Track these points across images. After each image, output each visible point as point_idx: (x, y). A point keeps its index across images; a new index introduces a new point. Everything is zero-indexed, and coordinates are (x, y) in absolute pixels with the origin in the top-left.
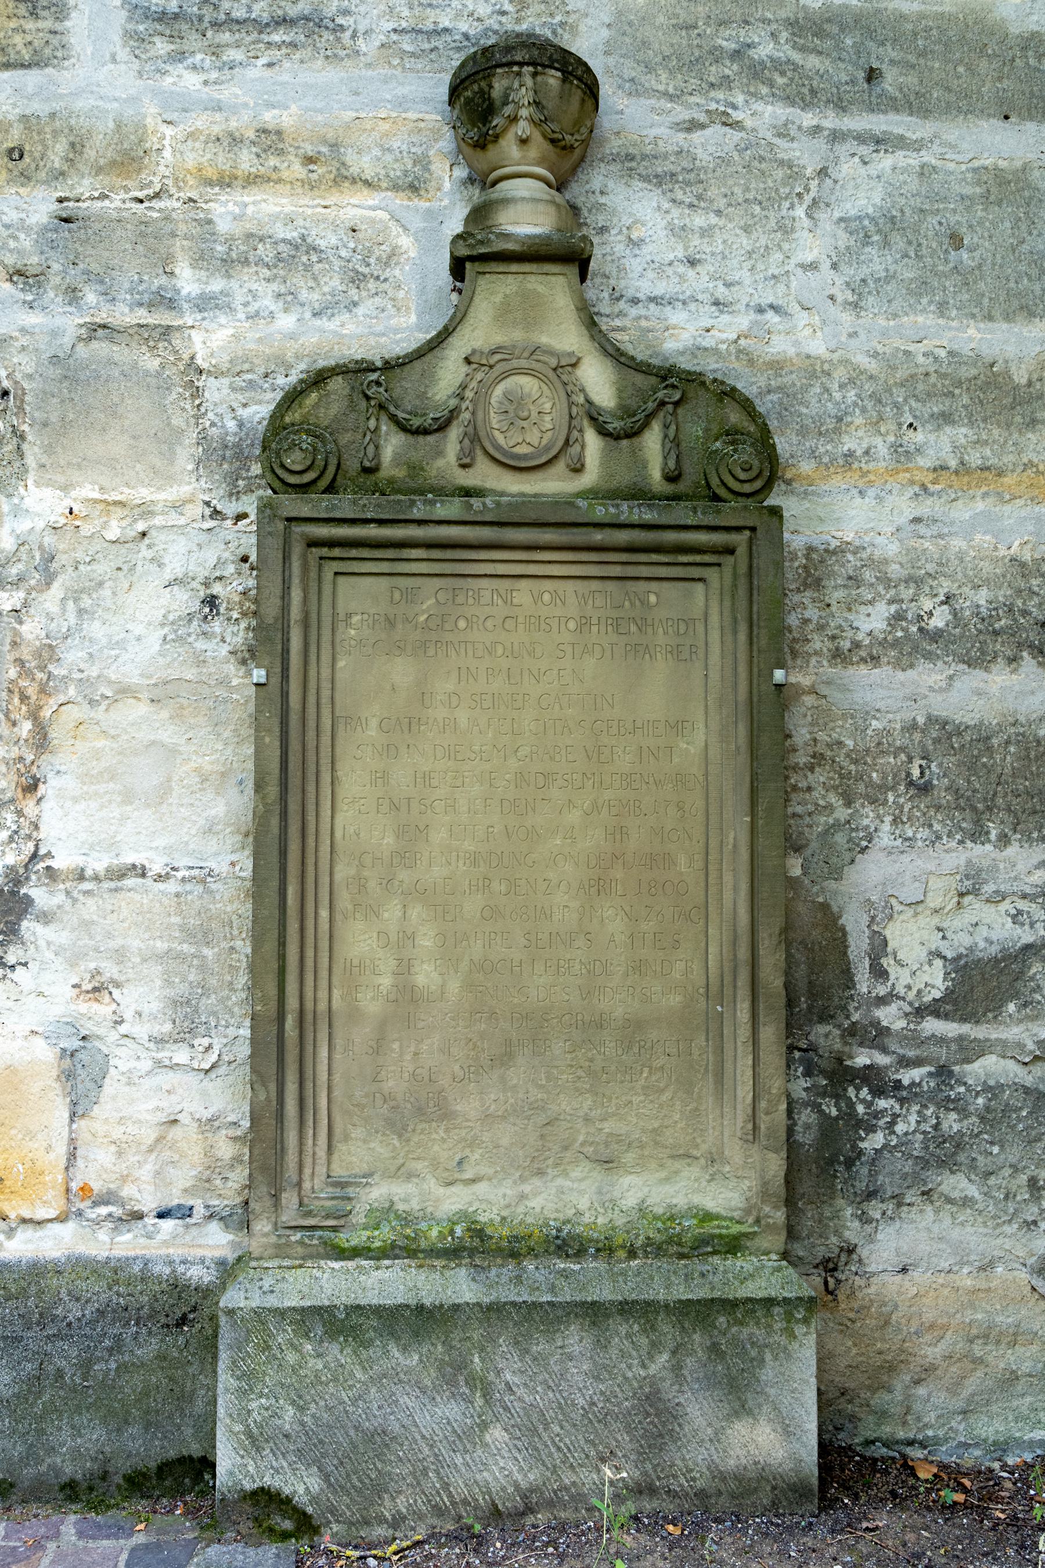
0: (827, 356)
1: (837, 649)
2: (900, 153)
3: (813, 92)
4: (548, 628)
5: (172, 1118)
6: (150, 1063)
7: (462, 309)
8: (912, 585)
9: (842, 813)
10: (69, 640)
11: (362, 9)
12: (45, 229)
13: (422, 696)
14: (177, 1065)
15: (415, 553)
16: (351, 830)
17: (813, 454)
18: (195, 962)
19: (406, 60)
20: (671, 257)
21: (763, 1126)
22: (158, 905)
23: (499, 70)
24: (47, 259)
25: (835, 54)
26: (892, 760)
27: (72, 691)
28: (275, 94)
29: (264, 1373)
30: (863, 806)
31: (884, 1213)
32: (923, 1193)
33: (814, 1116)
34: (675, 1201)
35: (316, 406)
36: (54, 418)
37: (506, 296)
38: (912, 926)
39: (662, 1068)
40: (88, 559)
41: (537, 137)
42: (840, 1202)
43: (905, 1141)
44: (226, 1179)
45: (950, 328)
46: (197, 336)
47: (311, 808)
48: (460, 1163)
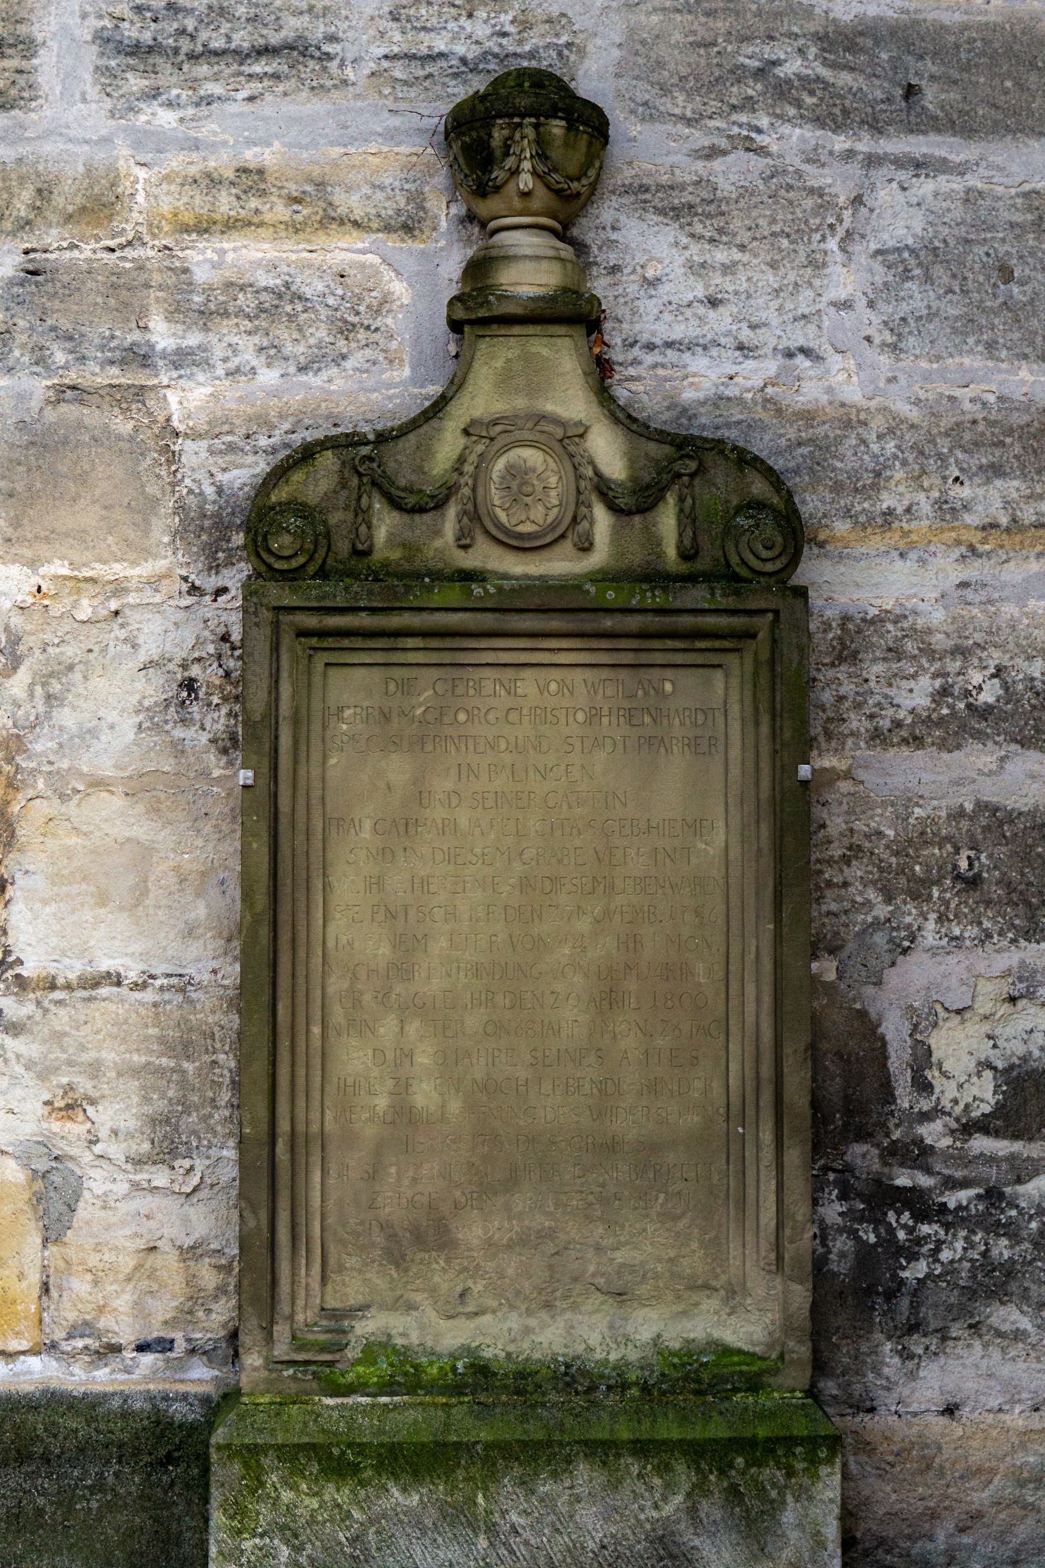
0: (865, 404)
1: (876, 729)
2: (942, 178)
3: (845, 112)
4: (555, 720)
5: (152, 1245)
6: (127, 1186)
7: (460, 374)
8: (959, 657)
9: (882, 911)
10: (38, 729)
11: (350, 34)
12: (11, 283)
13: (420, 795)
14: (156, 1188)
15: (411, 642)
16: (344, 939)
17: (847, 513)
18: (175, 1077)
19: (398, 88)
20: (690, 296)
21: (787, 1256)
22: (134, 1016)
23: (499, 121)
24: (13, 316)
25: (869, 70)
26: (937, 851)
27: (41, 784)
28: (256, 130)
29: (258, 1514)
30: (905, 902)
31: (927, 1348)
32: (970, 1326)
33: (851, 1243)
34: (692, 1336)
35: (305, 483)
36: (19, 487)
37: (508, 361)
38: (959, 1035)
39: (679, 1193)
40: (56, 641)
41: (541, 192)
42: (879, 1336)
43: (951, 1268)
44: (209, 1311)
45: (1000, 371)
46: (173, 398)
47: (301, 916)
48: (462, 1295)
